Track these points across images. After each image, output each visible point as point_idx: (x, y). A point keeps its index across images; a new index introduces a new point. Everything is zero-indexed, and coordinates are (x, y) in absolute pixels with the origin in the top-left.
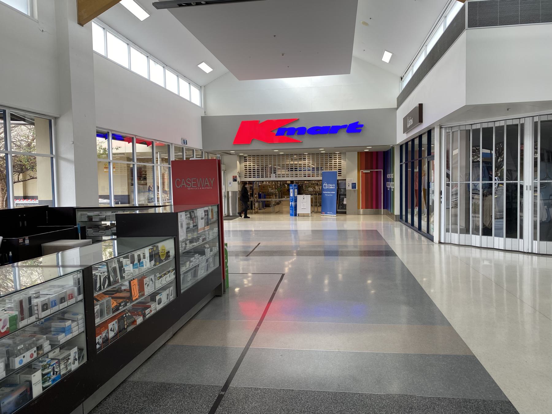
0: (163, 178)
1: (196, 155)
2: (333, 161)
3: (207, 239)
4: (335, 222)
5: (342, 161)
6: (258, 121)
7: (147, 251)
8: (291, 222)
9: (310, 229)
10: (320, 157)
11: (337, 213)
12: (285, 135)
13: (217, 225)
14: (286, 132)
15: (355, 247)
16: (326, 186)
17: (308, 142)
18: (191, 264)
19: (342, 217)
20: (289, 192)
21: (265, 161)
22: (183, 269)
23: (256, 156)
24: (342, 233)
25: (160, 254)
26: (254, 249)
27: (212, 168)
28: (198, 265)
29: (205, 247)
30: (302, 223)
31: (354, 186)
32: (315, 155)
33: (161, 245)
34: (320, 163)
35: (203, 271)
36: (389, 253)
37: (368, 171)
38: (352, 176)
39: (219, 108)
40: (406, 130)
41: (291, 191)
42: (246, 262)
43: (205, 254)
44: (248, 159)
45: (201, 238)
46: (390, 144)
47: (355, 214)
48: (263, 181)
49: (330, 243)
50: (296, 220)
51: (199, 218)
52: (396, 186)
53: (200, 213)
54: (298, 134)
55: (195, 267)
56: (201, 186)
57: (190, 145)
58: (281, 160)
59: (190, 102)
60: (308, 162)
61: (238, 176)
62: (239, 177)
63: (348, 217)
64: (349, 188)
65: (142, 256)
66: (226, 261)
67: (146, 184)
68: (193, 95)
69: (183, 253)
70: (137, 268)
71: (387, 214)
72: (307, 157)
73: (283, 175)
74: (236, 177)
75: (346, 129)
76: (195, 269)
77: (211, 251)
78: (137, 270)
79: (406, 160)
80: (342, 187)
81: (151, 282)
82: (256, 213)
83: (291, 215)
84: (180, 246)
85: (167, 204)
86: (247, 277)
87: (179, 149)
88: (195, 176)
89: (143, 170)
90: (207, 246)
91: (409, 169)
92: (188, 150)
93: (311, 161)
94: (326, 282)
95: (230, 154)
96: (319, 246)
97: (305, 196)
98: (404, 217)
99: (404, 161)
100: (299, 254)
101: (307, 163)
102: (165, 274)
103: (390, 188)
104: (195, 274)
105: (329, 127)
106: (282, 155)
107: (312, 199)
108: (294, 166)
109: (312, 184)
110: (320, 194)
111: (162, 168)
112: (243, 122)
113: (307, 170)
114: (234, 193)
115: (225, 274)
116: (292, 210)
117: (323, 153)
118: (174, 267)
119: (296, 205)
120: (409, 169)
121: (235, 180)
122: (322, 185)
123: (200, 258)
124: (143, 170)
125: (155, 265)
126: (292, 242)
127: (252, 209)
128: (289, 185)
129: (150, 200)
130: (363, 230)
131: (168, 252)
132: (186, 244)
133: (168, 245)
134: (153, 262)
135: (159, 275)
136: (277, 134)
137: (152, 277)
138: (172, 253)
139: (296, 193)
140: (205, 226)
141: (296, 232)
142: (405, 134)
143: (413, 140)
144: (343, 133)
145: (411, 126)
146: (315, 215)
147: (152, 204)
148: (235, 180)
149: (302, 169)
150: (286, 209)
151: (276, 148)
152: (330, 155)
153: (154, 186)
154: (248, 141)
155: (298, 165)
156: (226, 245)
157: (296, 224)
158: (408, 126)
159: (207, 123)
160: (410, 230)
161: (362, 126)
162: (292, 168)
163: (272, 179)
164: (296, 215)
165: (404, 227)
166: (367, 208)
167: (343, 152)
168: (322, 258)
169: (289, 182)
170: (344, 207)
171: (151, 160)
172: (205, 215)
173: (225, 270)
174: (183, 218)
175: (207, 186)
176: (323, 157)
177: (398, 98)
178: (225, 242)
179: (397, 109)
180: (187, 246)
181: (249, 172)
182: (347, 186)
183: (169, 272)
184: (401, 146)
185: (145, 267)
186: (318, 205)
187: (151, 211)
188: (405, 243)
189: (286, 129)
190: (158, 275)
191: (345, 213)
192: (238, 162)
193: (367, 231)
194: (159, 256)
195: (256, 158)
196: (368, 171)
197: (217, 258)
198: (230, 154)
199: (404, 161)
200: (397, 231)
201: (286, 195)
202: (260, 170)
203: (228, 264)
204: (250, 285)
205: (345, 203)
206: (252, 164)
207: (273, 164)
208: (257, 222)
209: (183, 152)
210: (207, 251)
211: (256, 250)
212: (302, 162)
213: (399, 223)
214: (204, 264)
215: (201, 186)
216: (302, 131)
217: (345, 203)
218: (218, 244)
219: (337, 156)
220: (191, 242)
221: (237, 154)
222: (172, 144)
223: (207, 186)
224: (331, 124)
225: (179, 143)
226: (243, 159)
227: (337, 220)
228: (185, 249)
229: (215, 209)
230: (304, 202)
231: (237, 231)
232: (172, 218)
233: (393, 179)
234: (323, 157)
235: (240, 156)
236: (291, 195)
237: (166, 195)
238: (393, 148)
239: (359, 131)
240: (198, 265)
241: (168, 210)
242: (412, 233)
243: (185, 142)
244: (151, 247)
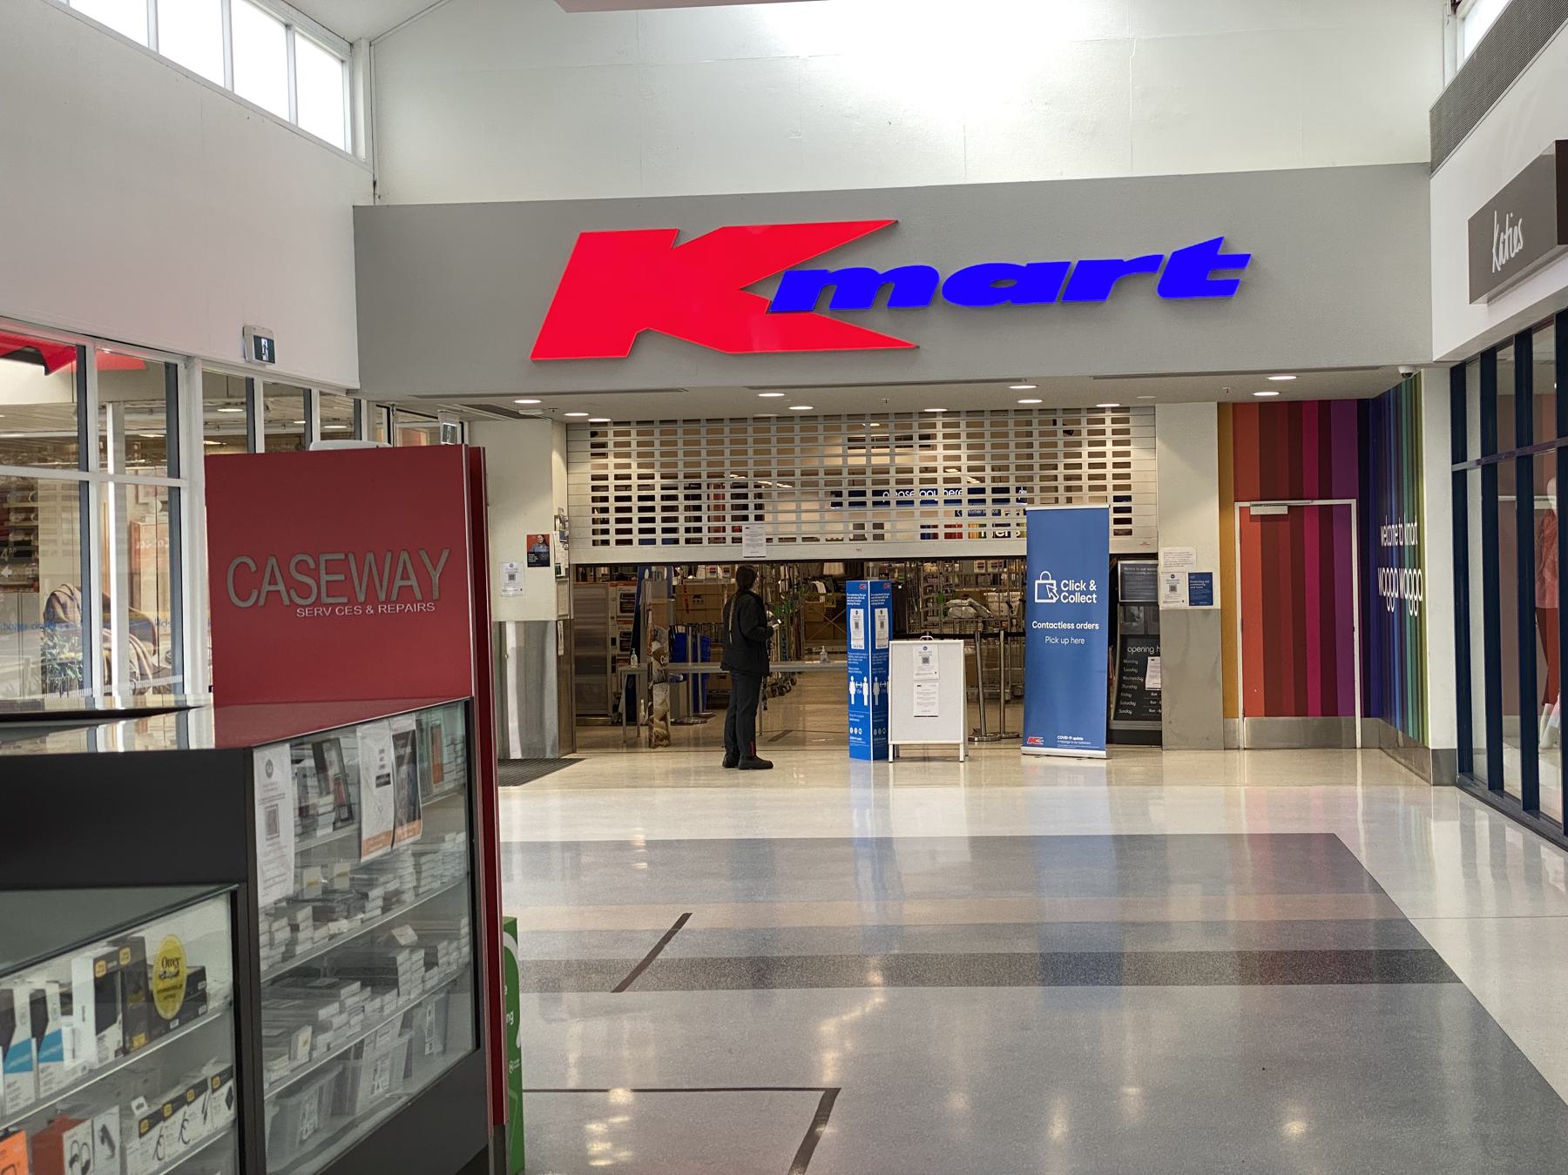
0: (132, 552)
1: (324, 421)
2: (1085, 450)
3: (408, 897)
4: (1103, 789)
5: (1136, 454)
6: (672, 234)
7: (81, 970)
8: (856, 793)
9: (963, 830)
10: (1011, 428)
11: (1113, 738)
12: (823, 308)
13: (460, 813)
14: (828, 294)
15: (1213, 928)
16: (1049, 588)
17: (953, 349)
18: (323, 1039)
19: (1135, 762)
20: (844, 620)
21: (716, 456)
22: (277, 1073)
23: (660, 425)
24: (1136, 853)
25: (155, 985)
26: (658, 948)
27: (443, 494)
28: (359, 1048)
29: (392, 943)
30: (912, 797)
31: (1200, 588)
32: (988, 417)
33: (157, 938)
34: (1012, 461)
35: (383, 1082)
36: (1401, 961)
37: (1279, 509)
38: (1189, 527)
39: (441, 165)
40: (1486, 281)
41: (856, 616)
42: (600, 1026)
43: (394, 984)
44: (611, 439)
45: (376, 893)
46: (1400, 360)
47: (1207, 745)
48: (692, 567)
49: (1075, 908)
50: (882, 783)
51: (369, 778)
52: (1432, 592)
53: (372, 747)
54: (896, 302)
55: (343, 1057)
56: (372, 598)
57: (291, 364)
58: (797, 446)
59: (291, 130)
60: (945, 458)
61: (555, 538)
62: (565, 539)
63: (1171, 759)
64: (1172, 598)
65: (53, 1004)
66: (510, 1017)
67: (33, 584)
68: (314, 94)
69: (274, 981)
70: (25, 1067)
71: (1387, 745)
72: (940, 431)
73: (798, 529)
74: (546, 540)
75: (1157, 277)
76: (340, 1075)
77: (430, 963)
78: (25, 1080)
79: (1488, 446)
80: (1134, 593)
81: (103, 1150)
82: (660, 742)
83: (857, 753)
84: (263, 939)
85: (153, 701)
86: (607, 1111)
87: (232, 389)
88: (336, 538)
89: (12, 503)
90: (406, 935)
91: (1507, 498)
92: (277, 390)
93: (963, 453)
94: (1058, 1129)
95: (514, 414)
96: (1020, 929)
97: (934, 645)
98: (1481, 763)
99: (1474, 451)
100: (908, 970)
101: (940, 464)
102: (179, 1103)
103: (1401, 602)
104: (341, 1099)
105: (1067, 264)
106: (805, 417)
107: (969, 660)
108: (869, 477)
109: (965, 580)
110: (1018, 634)
111: (130, 491)
112: (584, 238)
113: (937, 503)
114: (533, 631)
115: (508, 1092)
116: (862, 724)
117: (1028, 410)
118: (228, 1062)
119: (883, 696)
120: (1507, 498)
121: (538, 558)
122: (1024, 583)
123: (369, 1007)
124: (12, 503)
125: (124, 1051)
126: (851, 910)
127: (632, 718)
128: (836, 585)
129: (53, 675)
130: (1254, 838)
131: (199, 975)
132: (295, 928)
133: (195, 934)
134: (114, 1034)
135: (146, 1110)
136: (781, 304)
137: (110, 1119)
138: (219, 981)
139: (883, 632)
140: (398, 823)
141: (883, 847)
142: (1481, 306)
143: (1523, 340)
144: (1137, 302)
145: (1513, 265)
146: (983, 750)
147: (72, 701)
148: (538, 558)
149: (916, 496)
150: (816, 716)
151: (774, 380)
152: (1064, 418)
153: (85, 588)
154: (614, 343)
155: (893, 476)
156: (512, 927)
157: (883, 806)
158: (1499, 261)
159: (388, 247)
160: (1515, 835)
161: (1241, 261)
162: (853, 493)
163: (745, 552)
164: (881, 754)
165: (1484, 817)
166: (1272, 710)
167: (1138, 402)
168: (1031, 996)
169: (837, 570)
170: (1149, 705)
171: (73, 451)
172: (400, 760)
173: (508, 1067)
174: (276, 776)
175: (406, 594)
176: (1026, 433)
177: (1437, 112)
178: (508, 910)
179: (1433, 167)
180: (301, 936)
181: (611, 511)
182: (1163, 590)
183: (201, 1088)
184: (1458, 373)
185: (68, 1062)
186: (1005, 693)
187: (61, 743)
188: (1490, 907)
189: (823, 278)
190: (141, 1108)
191: (1154, 739)
192: (557, 459)
193: (1279, 843)
194: (150, 998)
195: (657, 438)
196: (1279, 509)
197: (465, 1002)
198: (514, 414)
199: (1474, 451)
200: (1444, 837)
201: (820, 639)
202: (681, 503)
203: (523, 1039)
204: (624, 1155)
205: (1152, 682)
206: (634, 471)
207: (751, 469)
208: (662, 797)
209: (250, 405)
210: (409, 964)
211: (668, 952)
212: (914, 458)
213: (1452, 794)
214: (390, 1041)
215: (372, 598)
216: (914, 287)
217: (1152, 682)
218: (465, 921)
219: (1108, 426)
220: (322, 915)
221: (551, 415)
222: (189, 359)
223: (406, 594)
224: (1072, 251)
225: (232, 354)
226: (583, 437)
227: (1112, 777)
228: (288, 955)
229: (451, 725)
230: (929, 683)
231: (545, 846)
232: (227, 772)
233: (1417, 551)
234: (1026, 433)
235: (570, 427)
236: (857, 640)
237: (148, 647)
238: (1412, 380)
239: (1228, 289)
240: (359, 1048)
241: (202, 734)
242: (1532, 852)
243: (263, 349)
244: (102, 948)
